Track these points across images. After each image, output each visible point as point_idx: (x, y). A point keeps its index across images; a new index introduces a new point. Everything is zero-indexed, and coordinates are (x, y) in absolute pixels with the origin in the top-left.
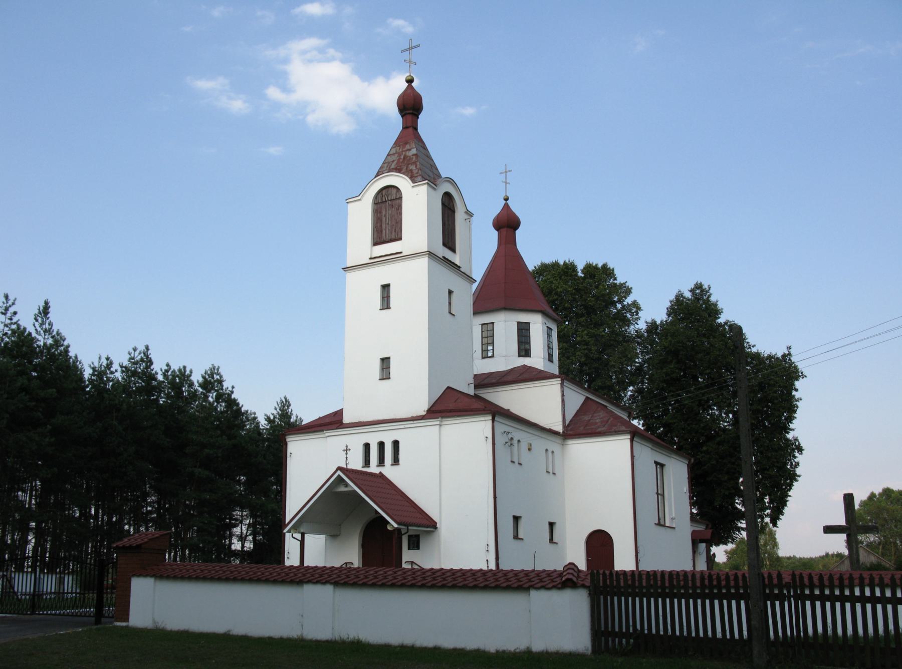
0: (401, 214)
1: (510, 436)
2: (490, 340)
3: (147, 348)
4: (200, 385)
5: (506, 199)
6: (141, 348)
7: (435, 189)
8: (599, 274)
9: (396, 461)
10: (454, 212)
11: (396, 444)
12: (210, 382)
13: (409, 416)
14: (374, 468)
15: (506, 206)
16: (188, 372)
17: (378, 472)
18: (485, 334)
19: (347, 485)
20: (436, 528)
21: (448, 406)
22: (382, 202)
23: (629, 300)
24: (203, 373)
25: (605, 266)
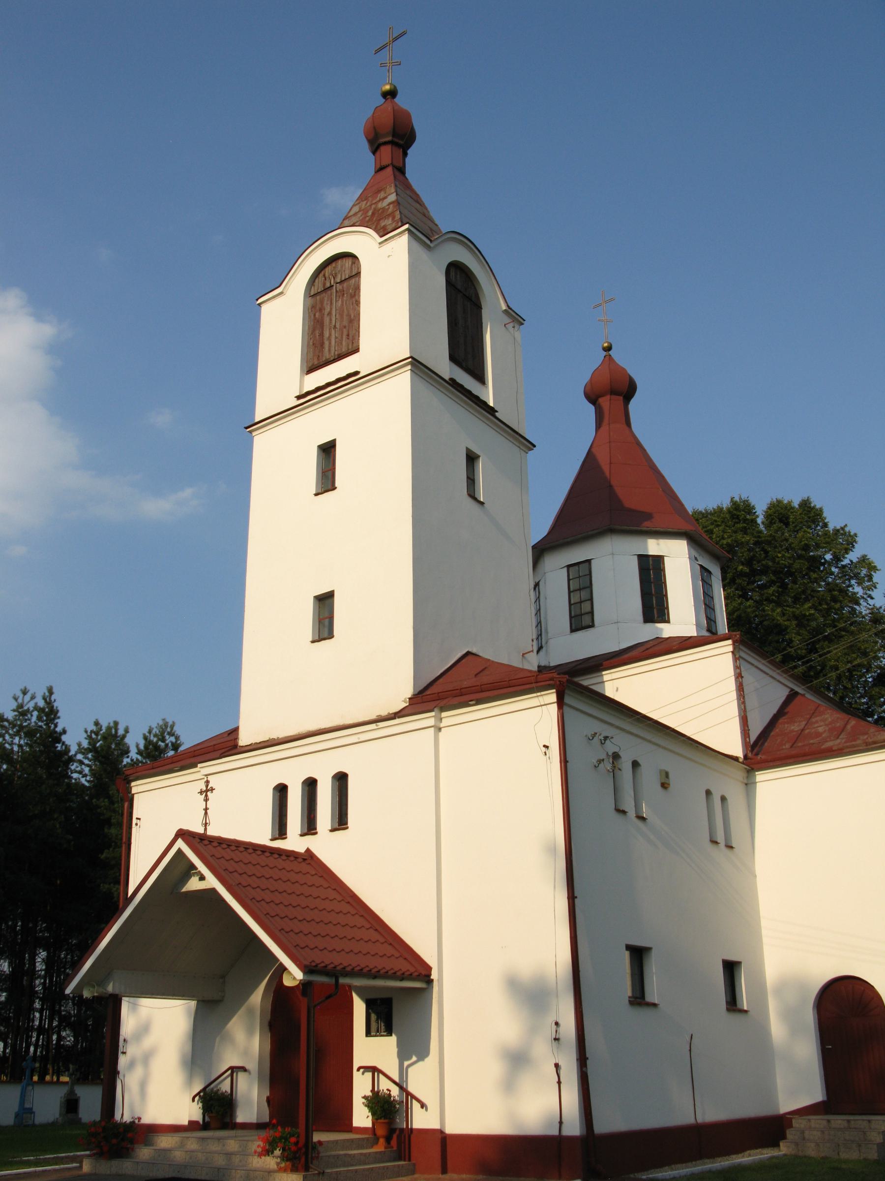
0: (358, 303)
1: (611, 748)
2: (584, 594)
3: (51, 691)
4: (140, 752)
5: (609, 349)
6: (40, 692)
7: (428, 247)
8: (797, 521)
9: (341, 821)
10: (479, 307)
11: (341, 779)
12: (156, 747)
13: (373, 717)
14: (295, 842)
15: (609, 359)
16: (121, 732)
17: (301, 849)
18: (586, 607)
19: (202, 878)
20: (430, 982)
21: (451, 686)
22: (326, 290)
23: (853, 556)
24: (146, 731)
25: (805, 504)
